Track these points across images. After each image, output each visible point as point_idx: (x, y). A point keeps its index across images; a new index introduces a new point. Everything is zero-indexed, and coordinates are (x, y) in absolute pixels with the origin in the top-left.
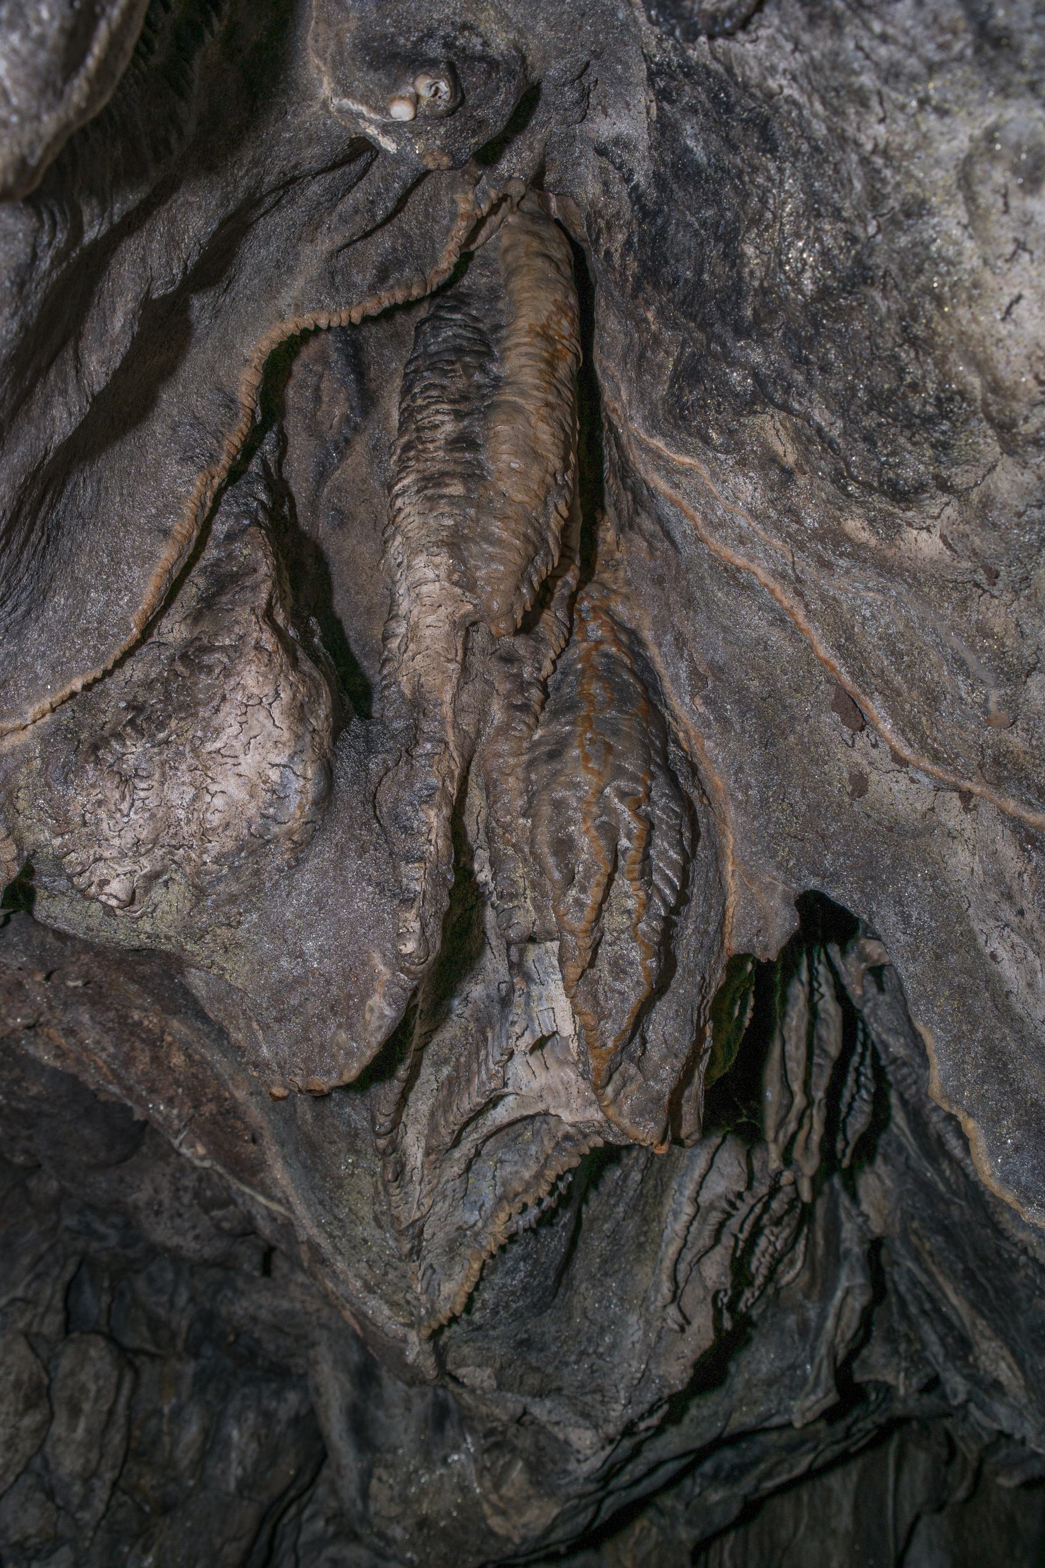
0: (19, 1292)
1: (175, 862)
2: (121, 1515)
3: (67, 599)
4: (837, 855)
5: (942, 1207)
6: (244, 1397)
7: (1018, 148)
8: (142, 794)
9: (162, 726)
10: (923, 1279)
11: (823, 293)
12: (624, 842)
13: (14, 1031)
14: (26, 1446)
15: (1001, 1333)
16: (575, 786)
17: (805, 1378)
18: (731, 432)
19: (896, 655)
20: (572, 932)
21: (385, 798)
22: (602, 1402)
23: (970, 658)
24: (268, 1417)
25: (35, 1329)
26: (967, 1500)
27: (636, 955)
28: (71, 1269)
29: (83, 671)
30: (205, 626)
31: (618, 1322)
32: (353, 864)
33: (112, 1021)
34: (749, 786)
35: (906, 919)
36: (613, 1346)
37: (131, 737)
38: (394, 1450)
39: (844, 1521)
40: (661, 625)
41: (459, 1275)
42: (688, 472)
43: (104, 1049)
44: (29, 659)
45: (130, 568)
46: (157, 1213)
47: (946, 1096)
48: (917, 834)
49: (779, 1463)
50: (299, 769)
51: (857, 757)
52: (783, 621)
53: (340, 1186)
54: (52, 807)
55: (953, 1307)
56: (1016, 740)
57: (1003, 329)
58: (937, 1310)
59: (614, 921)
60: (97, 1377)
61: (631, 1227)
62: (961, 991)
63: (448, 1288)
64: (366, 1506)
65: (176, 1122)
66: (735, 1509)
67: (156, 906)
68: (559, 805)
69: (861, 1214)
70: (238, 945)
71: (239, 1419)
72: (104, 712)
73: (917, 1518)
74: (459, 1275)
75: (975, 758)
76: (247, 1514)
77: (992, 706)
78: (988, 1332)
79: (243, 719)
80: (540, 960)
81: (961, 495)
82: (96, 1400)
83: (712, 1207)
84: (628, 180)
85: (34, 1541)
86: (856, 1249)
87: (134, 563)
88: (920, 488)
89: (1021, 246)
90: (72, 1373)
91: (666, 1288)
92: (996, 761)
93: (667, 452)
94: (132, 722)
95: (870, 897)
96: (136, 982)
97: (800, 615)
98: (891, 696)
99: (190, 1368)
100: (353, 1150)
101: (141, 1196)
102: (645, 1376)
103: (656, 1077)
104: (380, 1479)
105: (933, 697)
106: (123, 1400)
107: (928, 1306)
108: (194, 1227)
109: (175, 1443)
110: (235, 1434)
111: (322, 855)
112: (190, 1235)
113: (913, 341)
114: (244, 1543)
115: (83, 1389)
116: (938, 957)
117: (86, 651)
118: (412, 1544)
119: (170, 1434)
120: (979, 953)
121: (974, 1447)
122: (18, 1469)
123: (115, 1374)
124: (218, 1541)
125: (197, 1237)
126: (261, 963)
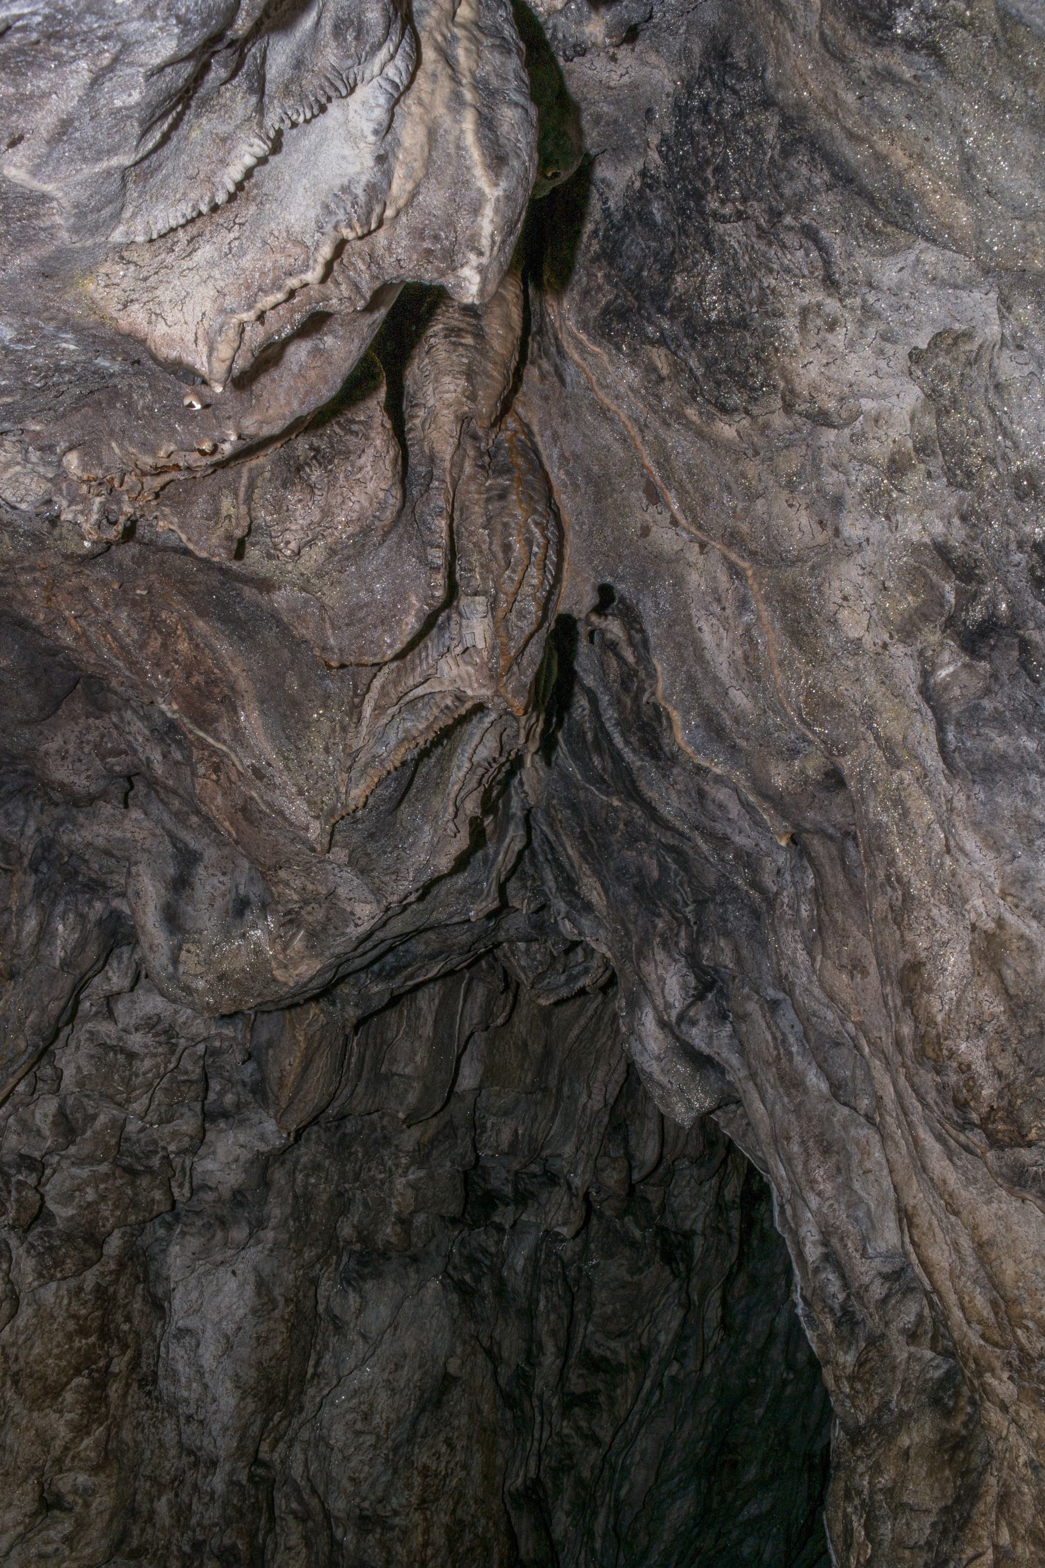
4: (626, 566)
5: (573, 791)
7: (828, 315)
9: (331, 462)
10: (552, 838)
11: (720, 322)
12: (535, 549)
15: (597, 873)
16: (514, 516)
17: (482, 890)
18: (635, 349)
19: (691, 474)
20: (505, 594)
21: (418, 510)
22: (395, 881)
23: (734, 486)
24: (82, 917)
26: (503, 1025)
27: (533, 609)
31: (419, 829)
32: (406, 546)
34: (583, 523)
35: (657, 605)
36: (413, 844)
38: (200, 932)
39: (427, 1031)
40: (543, 424)
41: (362, 786)
42: (594, 355)
46: (63, 758)
47: (665, 698)
48: (670, 562)
49: (420, 968)
50: (394, 493)
51: (647, 517)
52: (625, 441)
53: (308, 728)
55: (569, 857)
56: (744, 527)
57: (802, 371)
58: (556, 860)
59: (527, 589)
61: (435, 773)
62: (679, 646)
63: (355, 792)
64: (176, 969)
66: (386, 998)
68: (506, 525)
69: (524, 792)
70: (340, 583)
71: (63, 917)
73: (472, 1034)
74: (362, 786)
75: (721, 531)
76: (66, 982)
77: (738, 510)
78: (588, 872)
80: (468, 606)
81: (754, 418)
83: (479, 765)
84: (605, 203)
86: (519, 813)
88: (736, 410)
89: (818, 346)
91: (451, 809)
92: (731, 535)
93: (587, 343)
94: (314, 457)
95: (639, 591)
97: (639, 440)
98: (682, 493)
99: (32, 879)
100: (325, 706)
101: (52, 746)
102: (427, 865)
103: (525, 674)
104: (188, 951)
105: (706, 499)
107: (550, 857)
109: (19, 931)
110: (61, 927)
111: (394, 537)
112: (83, 776)
113: (758, 359)
114: (62, 1003)
116: (670, 626)
118: (211, 991)
119: (17, 924)
120: (692, 627)
121: (530, 974)
124: (46, 999)
125: (88, 777)
126: (348, 594)
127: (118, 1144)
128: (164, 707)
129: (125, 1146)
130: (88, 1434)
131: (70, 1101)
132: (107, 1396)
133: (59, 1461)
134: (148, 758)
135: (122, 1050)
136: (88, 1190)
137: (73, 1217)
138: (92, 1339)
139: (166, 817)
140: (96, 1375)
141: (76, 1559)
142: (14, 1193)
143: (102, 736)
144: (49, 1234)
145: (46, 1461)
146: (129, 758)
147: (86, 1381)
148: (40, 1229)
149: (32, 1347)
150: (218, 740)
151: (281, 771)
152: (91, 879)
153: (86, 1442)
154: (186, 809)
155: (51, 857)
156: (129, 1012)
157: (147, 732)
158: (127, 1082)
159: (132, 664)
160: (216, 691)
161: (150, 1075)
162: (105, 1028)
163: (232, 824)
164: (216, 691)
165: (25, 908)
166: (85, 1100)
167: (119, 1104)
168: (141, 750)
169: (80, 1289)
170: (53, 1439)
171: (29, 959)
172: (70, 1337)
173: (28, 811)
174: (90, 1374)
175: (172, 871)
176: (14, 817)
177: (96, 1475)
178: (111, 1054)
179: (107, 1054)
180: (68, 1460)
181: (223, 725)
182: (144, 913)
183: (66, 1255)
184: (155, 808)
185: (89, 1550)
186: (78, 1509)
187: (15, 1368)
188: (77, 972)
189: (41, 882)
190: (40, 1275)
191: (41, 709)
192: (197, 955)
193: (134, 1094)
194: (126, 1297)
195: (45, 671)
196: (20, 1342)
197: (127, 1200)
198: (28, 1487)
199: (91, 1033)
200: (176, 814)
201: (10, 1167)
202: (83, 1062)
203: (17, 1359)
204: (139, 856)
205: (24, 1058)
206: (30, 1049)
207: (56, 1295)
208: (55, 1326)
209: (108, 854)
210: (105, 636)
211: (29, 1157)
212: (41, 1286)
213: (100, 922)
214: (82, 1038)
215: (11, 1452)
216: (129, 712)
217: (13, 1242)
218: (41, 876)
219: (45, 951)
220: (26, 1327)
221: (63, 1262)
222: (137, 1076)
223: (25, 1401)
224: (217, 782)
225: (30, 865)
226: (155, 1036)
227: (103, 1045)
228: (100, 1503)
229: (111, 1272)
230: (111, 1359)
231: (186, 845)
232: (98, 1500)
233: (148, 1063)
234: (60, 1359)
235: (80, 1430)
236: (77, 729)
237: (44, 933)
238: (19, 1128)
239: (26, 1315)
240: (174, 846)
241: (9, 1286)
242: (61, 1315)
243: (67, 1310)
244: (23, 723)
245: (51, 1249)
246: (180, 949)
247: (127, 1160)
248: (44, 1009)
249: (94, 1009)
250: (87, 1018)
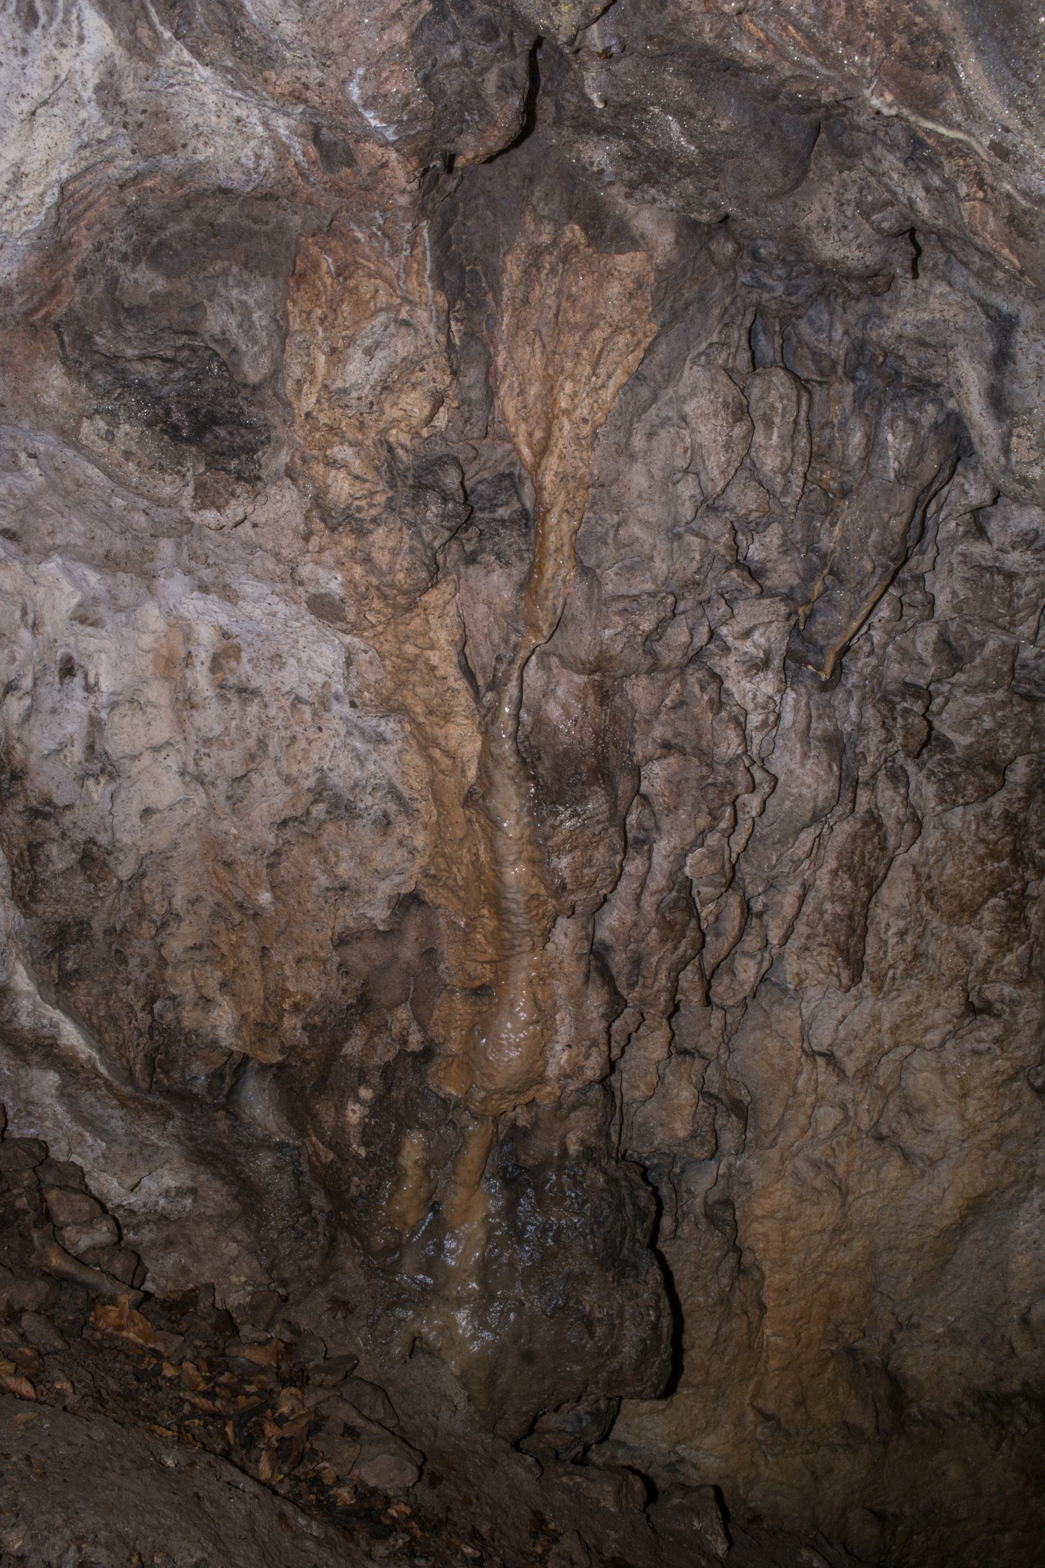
0: (715, 338)
2: (813, 497)
6: (894, 410)
14: (739, 450)
24: (914, 423)
25: (730, 365)
28: (749, 318)
38: (1030, 411)
46: (827, 229)
60: (781, 398)
64: (1008, 459)
65: (869, 70)
76: (905, 496)
82: (783, 416)
85: (754, 515)
90: (762, 398)
99: (850, 389)
101: (811, 218)
104: (1019, 436)
106: (803, 414)
108: (857, 237)
109: (845, 446)
110: (890, 437)
112: (854, 246)
114: (905, 517)
115: (772, 407)
119: (841, 438)
122: (737, 465)
123: (795, 393)
124: (885, 516)
127: (1013, 670)
128: (875, 102)
129: (1019, 673)
130: (1011, 950)
131: (953, 627)
132: (1026, 918)
133: (983, 973)
134: (909, 199)
135: (999, 571)
136: (985, 717)
137: (971, 744)
138: (1005, 863)
139: (972, 283)
140: (1013, 897)
141: (1008, 1059)
142: (899, 720)
143: (861, 190)
144: (948, 761)
145: (969, 972)
146: (896, 208)
147: (1002, 902)
148: (939, 757)
149: (943, 868)
150: (950, 126)
151: (1021, 132)
152: (914, 379)
153: (1009, 958)
154: (988, 264)
155: (866, 360)
156: (1004, 529)
157: (901, 165)
158: (1008, 604)
159: (824, 54)
160: (927, 50)
161: (1034, 595)
162: (979, 549)
163: (1011, 249)
164: (927, 50)
165: (847, 420)
166: (969, 627)
167: (1003, 628)
168: (900, 191)
169: (987, 816)
170: (975, 952)
171: (859, 474)
172: (981, 860)
173: (831, 314)
174: (1006, 896)
175: (991, 347)
176: (818, 323)
177: (1022, 988)
178: (988, 576)
179: (982, 576)
180: (992, 972)
181: (952, 101)
182: (969, 403)
183: (966, 781)
184: (959, 275)
185: (1019, 1053)
186: (1006, 1016)
187: (928, 886)
188: (917, 484)
189: (860, 390)
190: (942, 801)
191: (786, 173)
192: (1029, 438)
193: (1018, 617)
194: (1039, 824)
195: (773, 122)
196: (931, 862)
197: (1028, 728)
198: (954, 993)
199: (964, 555)
200: (978, 274)
201: (895, 695)
202: (958, 587)
203: (929, 877)
204: (954, 338)
205: (875, 580)
206: (879, 570)
207: (963, 819)
208: (965, 849)
209: (922, 343)
210: (785, 29)
211: (915, 686)
212: (945, 811)
213: (935, 427)
214: (954, 561)
215: (934, 960)
216: (879, 147)
217: (911, 768)
218: (859, 383)
219: (877, 464)
220: (935, 850)
221: (965, 788)
222: (1019, 596)
223: (942, 916)
224: (984, 200)
225: (845, 374)
226: (1033, 553)
227: (979, 567)
228: (1028, 1014)
229: (1019, 800)
230: (1027, 883)
231: (998, 310)
232: (1025, 1011)
233: (1030, 583)
234: (974, 880)
235: (1002, 947)
236: (832, 190)
237: (873, 445)
238: (899, 657)
239: (932, 838)
240: (988, 316)
241: (909, 810)
242: (970, 840)
243: (976, 835)
244: (773, 197)
245: (950, 775)
246: (1010, 435)
247: (1026, 687)
248: (885, 526)
249: (961, 529)
250: (953, 540)
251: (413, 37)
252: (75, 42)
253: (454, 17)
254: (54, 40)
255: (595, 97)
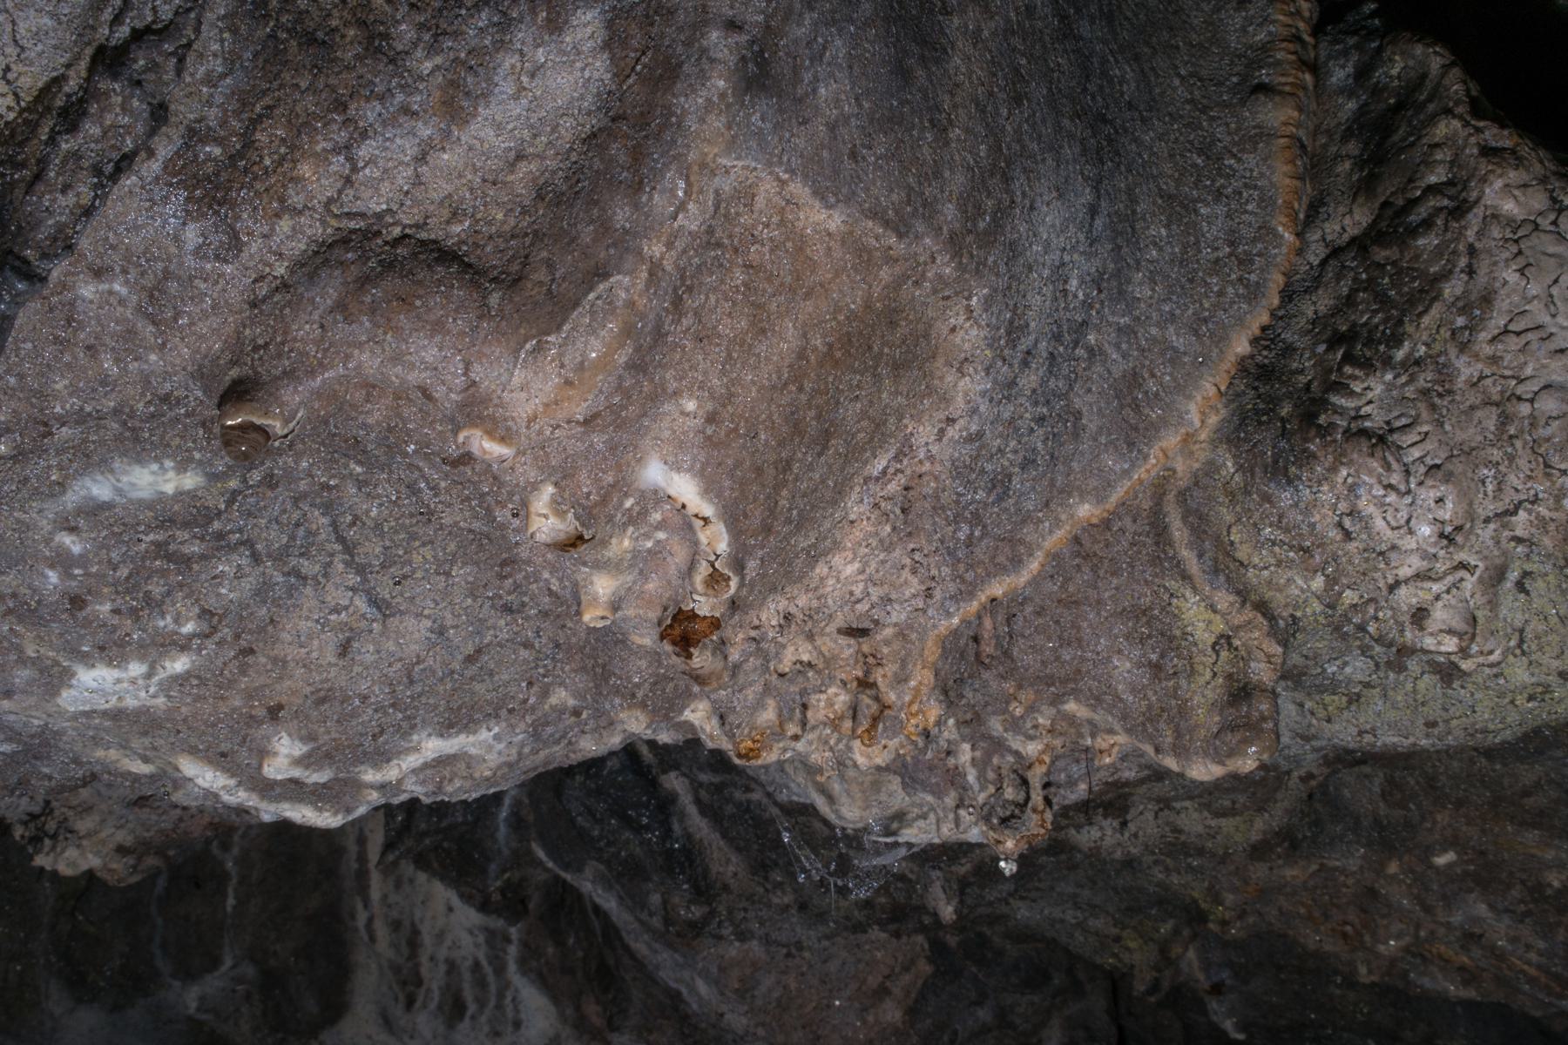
1: (1519, 540)
3: (1167, 226)
8: (1416, 453)
13: (1393, 962)
29: (1240, 322)
30: (1387, 189)
33: (1522, 901)
37: (1356, 378)
43: (1528, 947)
44: (1154, 331)
45: (1239, 160)
54: (1287, 530)
67: (1522, 631)
72: (1301, 372)
79: (1521, 261)
87: (1243, 151)
96: (1534, 826)
117: (1230, 290)
251: (912, 1012)
252: (510, 1029)
253: (974, 969)
254: (486, 1029)
255: (1228, 1025)
